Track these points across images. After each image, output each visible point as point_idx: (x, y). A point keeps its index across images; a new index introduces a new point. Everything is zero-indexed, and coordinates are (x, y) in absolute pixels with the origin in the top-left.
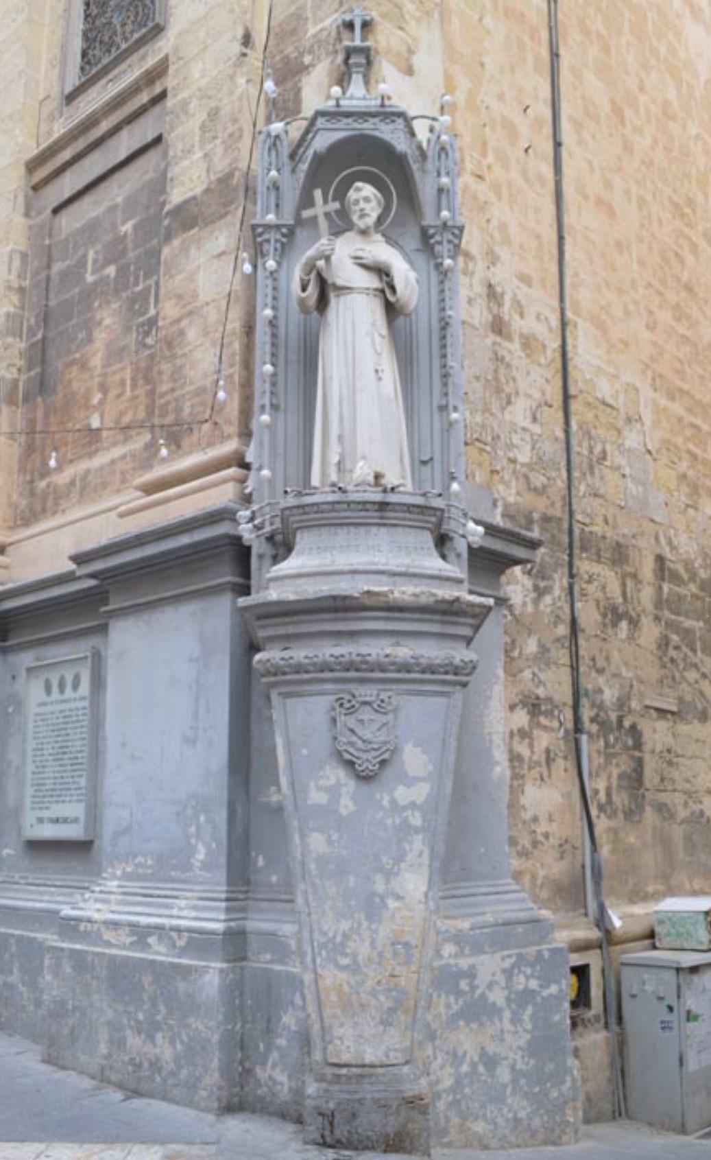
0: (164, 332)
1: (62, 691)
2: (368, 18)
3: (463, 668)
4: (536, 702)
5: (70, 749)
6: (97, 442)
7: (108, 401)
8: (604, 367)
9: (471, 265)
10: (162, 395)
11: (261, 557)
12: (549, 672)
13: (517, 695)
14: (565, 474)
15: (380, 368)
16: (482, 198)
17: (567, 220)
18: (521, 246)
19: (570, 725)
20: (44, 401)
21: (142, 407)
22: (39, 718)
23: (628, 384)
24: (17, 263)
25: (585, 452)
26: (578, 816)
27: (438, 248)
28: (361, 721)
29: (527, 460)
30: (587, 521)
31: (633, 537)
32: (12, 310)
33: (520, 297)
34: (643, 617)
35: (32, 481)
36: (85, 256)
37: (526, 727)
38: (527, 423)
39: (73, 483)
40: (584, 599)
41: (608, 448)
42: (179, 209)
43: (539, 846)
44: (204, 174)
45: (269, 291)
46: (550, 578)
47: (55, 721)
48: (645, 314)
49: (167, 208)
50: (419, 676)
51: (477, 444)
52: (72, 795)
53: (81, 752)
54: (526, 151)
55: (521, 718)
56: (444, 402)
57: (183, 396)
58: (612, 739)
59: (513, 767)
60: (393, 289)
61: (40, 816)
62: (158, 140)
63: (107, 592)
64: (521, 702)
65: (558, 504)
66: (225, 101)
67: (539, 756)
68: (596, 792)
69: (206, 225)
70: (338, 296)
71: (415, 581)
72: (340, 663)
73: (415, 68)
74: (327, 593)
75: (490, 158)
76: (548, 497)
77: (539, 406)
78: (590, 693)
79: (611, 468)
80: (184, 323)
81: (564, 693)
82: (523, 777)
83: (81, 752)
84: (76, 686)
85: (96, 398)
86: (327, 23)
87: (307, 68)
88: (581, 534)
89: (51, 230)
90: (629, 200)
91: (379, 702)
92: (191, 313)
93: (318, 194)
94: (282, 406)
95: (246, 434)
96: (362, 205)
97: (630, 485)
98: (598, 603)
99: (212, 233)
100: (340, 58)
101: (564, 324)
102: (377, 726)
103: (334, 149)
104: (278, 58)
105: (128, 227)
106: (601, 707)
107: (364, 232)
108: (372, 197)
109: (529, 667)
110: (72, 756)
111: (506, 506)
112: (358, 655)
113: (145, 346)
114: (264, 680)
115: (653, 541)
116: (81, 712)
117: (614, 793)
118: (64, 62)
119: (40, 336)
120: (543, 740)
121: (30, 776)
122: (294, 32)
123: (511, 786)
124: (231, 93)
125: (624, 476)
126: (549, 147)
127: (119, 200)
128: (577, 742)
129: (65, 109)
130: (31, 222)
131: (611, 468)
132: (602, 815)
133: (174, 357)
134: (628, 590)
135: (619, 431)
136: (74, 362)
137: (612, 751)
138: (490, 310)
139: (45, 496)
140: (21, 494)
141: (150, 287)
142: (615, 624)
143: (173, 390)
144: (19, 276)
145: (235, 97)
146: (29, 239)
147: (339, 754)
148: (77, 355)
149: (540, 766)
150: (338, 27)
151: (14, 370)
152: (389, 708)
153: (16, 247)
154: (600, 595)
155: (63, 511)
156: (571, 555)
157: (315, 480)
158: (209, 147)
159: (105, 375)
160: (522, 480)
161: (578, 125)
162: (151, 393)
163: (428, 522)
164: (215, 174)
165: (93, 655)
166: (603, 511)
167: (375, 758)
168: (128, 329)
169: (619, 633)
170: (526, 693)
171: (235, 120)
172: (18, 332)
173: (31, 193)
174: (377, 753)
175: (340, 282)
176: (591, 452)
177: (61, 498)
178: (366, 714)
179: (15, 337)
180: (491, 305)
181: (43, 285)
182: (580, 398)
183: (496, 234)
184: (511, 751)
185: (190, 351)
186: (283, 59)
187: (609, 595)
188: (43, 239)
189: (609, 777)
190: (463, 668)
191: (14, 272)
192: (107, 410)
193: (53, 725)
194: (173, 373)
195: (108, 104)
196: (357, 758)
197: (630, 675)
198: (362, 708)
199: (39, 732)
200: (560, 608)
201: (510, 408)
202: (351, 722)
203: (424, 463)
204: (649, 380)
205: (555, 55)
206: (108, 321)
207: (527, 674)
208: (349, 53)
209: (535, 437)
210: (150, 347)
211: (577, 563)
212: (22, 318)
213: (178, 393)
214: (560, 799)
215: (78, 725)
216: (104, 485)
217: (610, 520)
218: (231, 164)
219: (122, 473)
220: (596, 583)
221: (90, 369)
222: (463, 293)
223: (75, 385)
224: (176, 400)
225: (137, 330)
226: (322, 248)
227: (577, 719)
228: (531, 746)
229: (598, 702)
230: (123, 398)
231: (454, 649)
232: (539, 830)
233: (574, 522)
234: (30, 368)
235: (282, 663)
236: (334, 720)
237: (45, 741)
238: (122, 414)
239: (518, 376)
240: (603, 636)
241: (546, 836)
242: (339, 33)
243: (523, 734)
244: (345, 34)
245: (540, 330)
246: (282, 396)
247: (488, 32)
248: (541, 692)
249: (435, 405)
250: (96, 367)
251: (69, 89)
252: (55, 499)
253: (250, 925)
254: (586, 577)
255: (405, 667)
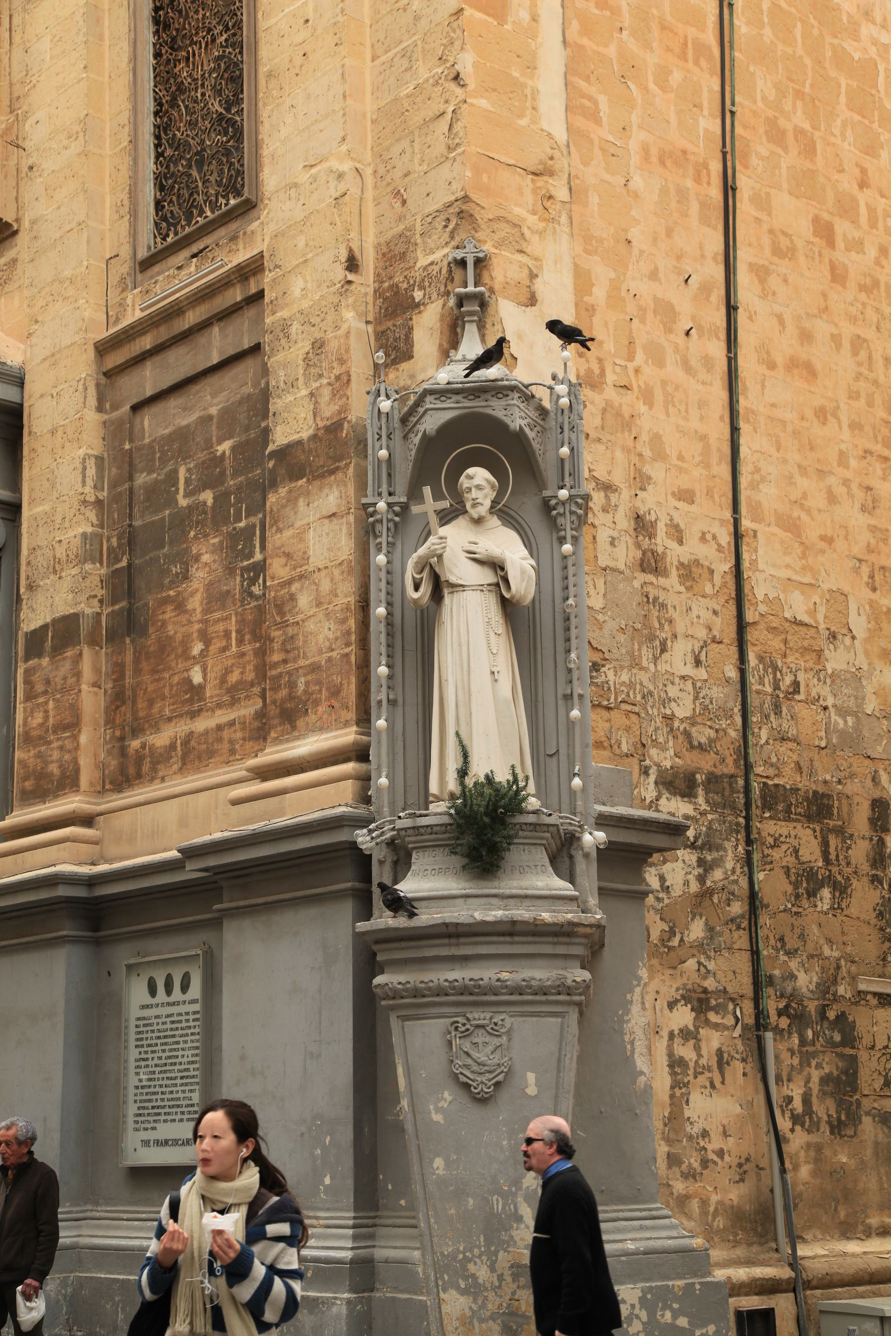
0: (273, 594)
1: (169, 991)
2: (481, 255)
3: (577, 989)
4: (703, 996)
5: (180, 1060)
6: (200, 700)
7: (211, 653)
8: (795, 577)
9: (614, 498)
10: (275, 665)
11: (381, 862)
12: (720, 960)
13: (677, 989)
14: (738, 720)
15: (495, 669)
16: (626, 412)
17: (743, 403)
18: (680, 457)
19: (750, 1021)
20: (132, 641)
21: (250, 667)
22: (141, 1023)
23: (831, 591)
24: (91, 471)
25: (769, 689)
26: (765, 1129)
27: (560, 521)
28: (475, 1044)
29: (688, 714)
30: (771, 772)
31: (839, 782)
32: (89, 530)
33: (678, 519)
34: (854, 882)
35: (122, 739)
36: (175, 472)
37: (691, 1028)
38: (689, 670)
39: (172, 747)
40: (768, 867)
41: (801, 677)
42: (282, 453)
43: (710, 1165)
44: (310, 417)
45: (383, 585)
46: (720, 848)
47: (161, 1027)
48: (859, 494)
49: (271, 448)
50: (530, 997)
51: (624, 706)
52: (183, 1113)
53: (193, 1062)
54: (687, 333)
55: (684, 1016)
56: (569, 692)
57: (297, 669)
58: (810, 1033)
59: (673, 1074)
60: (506, 580)
61: (145, 1138)
62: (256, 349)
63: (221, 888)
64: (683, 997)
65: (730, 761)
66: (330, 335)
67: (708, 1057)
68: (790, 1100)
69: (315, 478)
70: (452, 592)
71: (527, 902)
72: (454, 988)
73: (539, 296)
74: (439, 922)
75: (640, 358)
76: (717, 753)
77: (705, 644)
78: (777, 981)
79: (806, 702)
80: (295, 587)
81: (744, 984)
82: (687, 1085)
83: (193, 1062)
84: (185, 988)
85: (197, 648)
86: (437, 256)
87: (418, 305)
88: (761, 790)
89: (131, 431)
90: (839, 346)
91: (492, 1026)
92: (301, 577)
93: (427, 491)
94: (400, 700)
95: (364, 719)
96: (474, 494)
97: (834, 717)
98: (787, 870)
99: (321, 489)
100: (452, 302)
101: (737, 536)
102: (491, 1048)
103: (446, 429)
104: (386, 285)
105: (225, 447)
106: (794, 996)
107: (478, 521)
108: (484, 483)
109: (693, 956)
110: (182, 1067)
111: (661, 772)
112: (471, 980)
113: (251, 595)
114: (383, 1003)
115: (869, 783)
116: (191, 1017)
117: (814, 1100)
118: (134, 213)
119: (124, 563)
120: (712, 1040)
121: (131, 1091)
122: (403, 256)
123: (672, 1096)
124: (337, 328)
125: (825, 708)
126: (719, 318)
127: (214, 411)
128: (760, 1041)
129: (139, 277)
130: (106, 417)
131: (806, 702)
132: (798, 1128)
133: (284, 625)
134: (832, 850)
135: (819, 653)
136: (166, 601)
137: (811, 1049)
138: (638, 545)
139: (139, 759)
140: (109, 752)
141: (254, 526)
142: (812, 894)
143: (285, 661)
144: (95, 487)
145: (341, 332)
146: (104, 439)
147: (455, 1076)
148: (172, 593)
149: (709, 1069)
150: (449, 263)
151: (95, 602)
152: (503, 1030)
153: (90, 452)
154: (790, 860)
155: (163, 780)
156: (748, 818)
157: (434, 788)
158: (315, 385)
159: (205, 622)
160: (681, 738)
161: (761, 273)
162: (261, 653)
163: (542, 838)
164: (322, 419)
165: (205, 953)
166: (795, 757)
167: (490, 1080)
168: (230, 571)
169: (819, 904)
170: (690, 987)
171: (342, 361)
172: (98, 556)
173: (103, 380)
174: (492, 1076)
175: (453, 579)
176: (776, 687)
177: (159, 763)
178: (480, 1037)
179: (93, 563)
180: (641, 538)
181: (126, 497)
182: (762, 626)
183: (647, 453)
184: (670, 1055)
185: (303, 621)
186: (391, 287)
187: (803, 859)
188: (122, 443)
189: (808, 1081)
190: (577, 989)
191: (90, 482)
192: (210, 663)
193: (159, 1030)
194: (283, 643)
195: (196, 294)
196: (473, 1081)
197: (836, 954)
198: (477, 1031)
199: (142, 1039)
200: (736, 882)
201: (665, 656)
202: (467, 1046)
203: (551, 756)
204: (865, 578)
205: (729, 189)
206: (206, 558)
207: (691, 964)
208: (461, 300)
209: (699, 684)
210: (257, 598)
211: (756, 824)
212: (101, 536)
213: (290, 666)
214: (738, 1110)
215: (189, 1032)
216: (211, 754)
217: (805, 765)
218: (340, 413)
219: (231, 742)
220: (784, 847)
221: (186, 612)
222: (603, 535)
223: (171, 630)
224: (289, 673)
225: (242, 576)
226: (433, 547)
227: (760, 1014)
228: (697, 1049)
229: (789, 989)
230: (228, 653)
231: (565, 969)
232: (709, 1147)
233: (752, 777)
234: (114, 602)
235: (400, 986)
236: (450, 1043)
237: (150, 1049)
238: (228, 671)
239: (675, 615)
240: (794, 909)
241: (721, 1153)
242: (450, 271)
243: (686, 1034)
244: (458, 274)
245: (706, 553)
246: (399, 690)
247: (636, 196)
248: (710, 984)
249: (560, 695)
250: (194, 610)
251: (143, 253)
252: (151, 762)
253: (380, 1253)
254: (770, 840)
255: (517, 990)
